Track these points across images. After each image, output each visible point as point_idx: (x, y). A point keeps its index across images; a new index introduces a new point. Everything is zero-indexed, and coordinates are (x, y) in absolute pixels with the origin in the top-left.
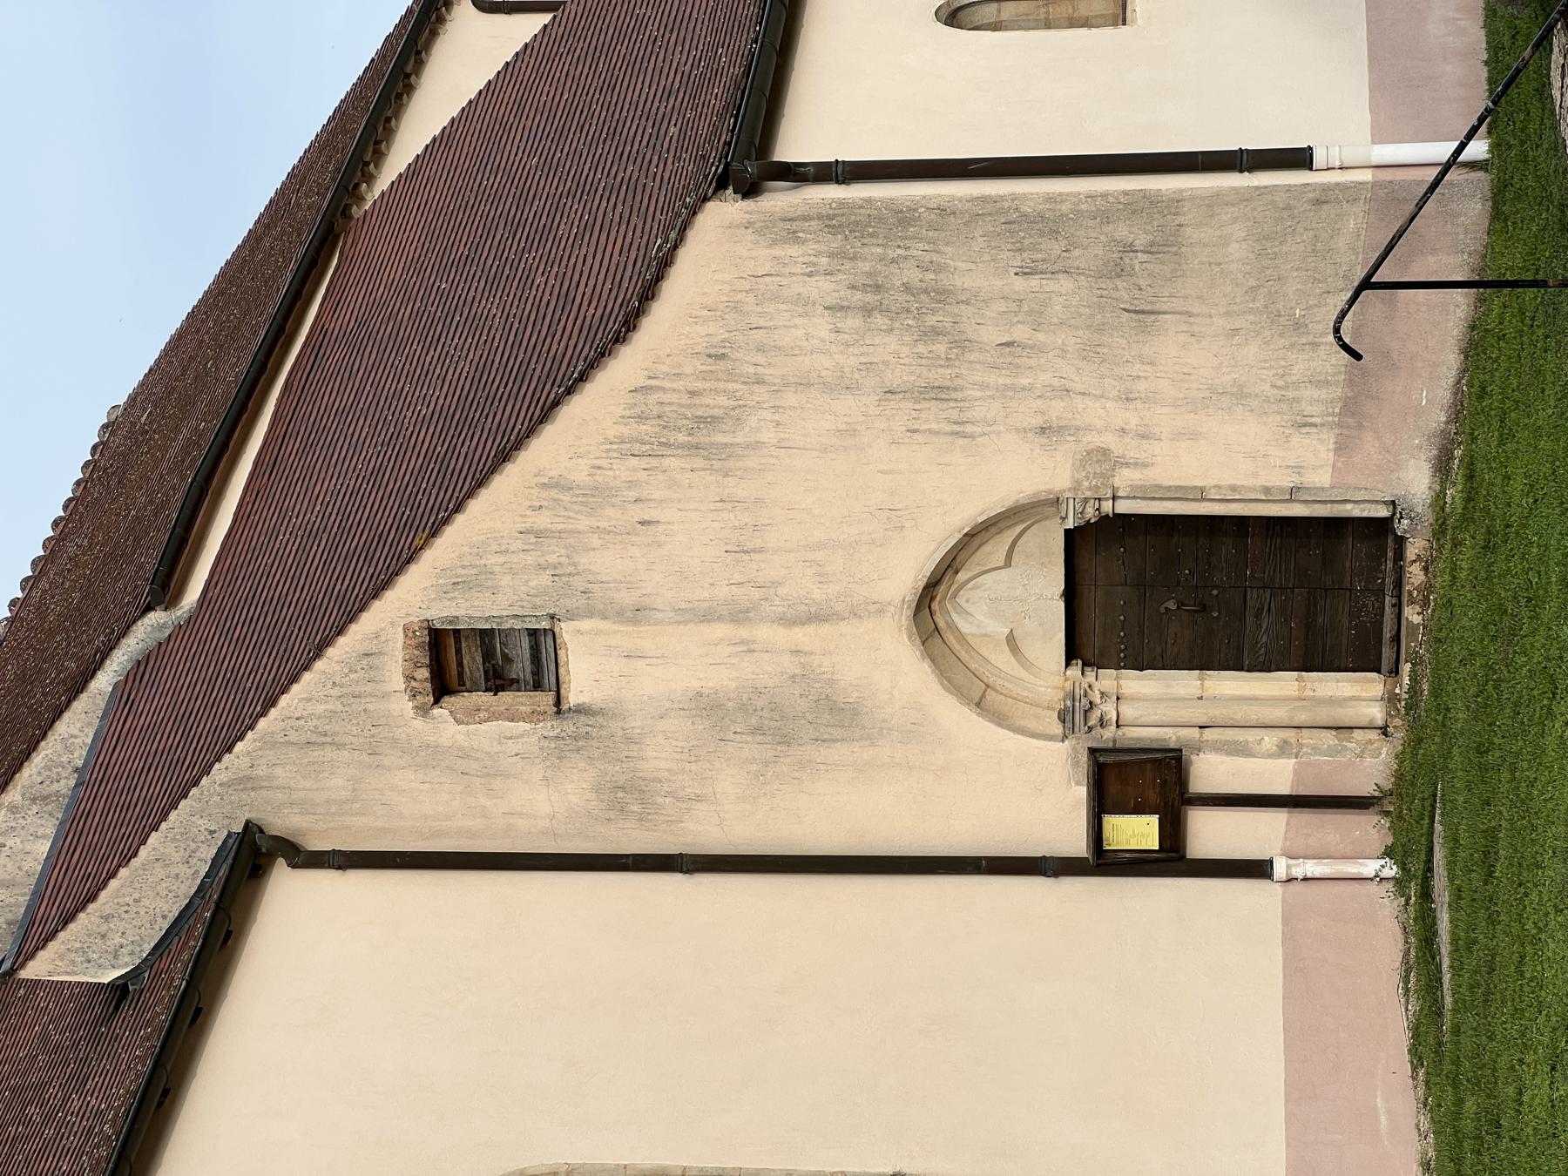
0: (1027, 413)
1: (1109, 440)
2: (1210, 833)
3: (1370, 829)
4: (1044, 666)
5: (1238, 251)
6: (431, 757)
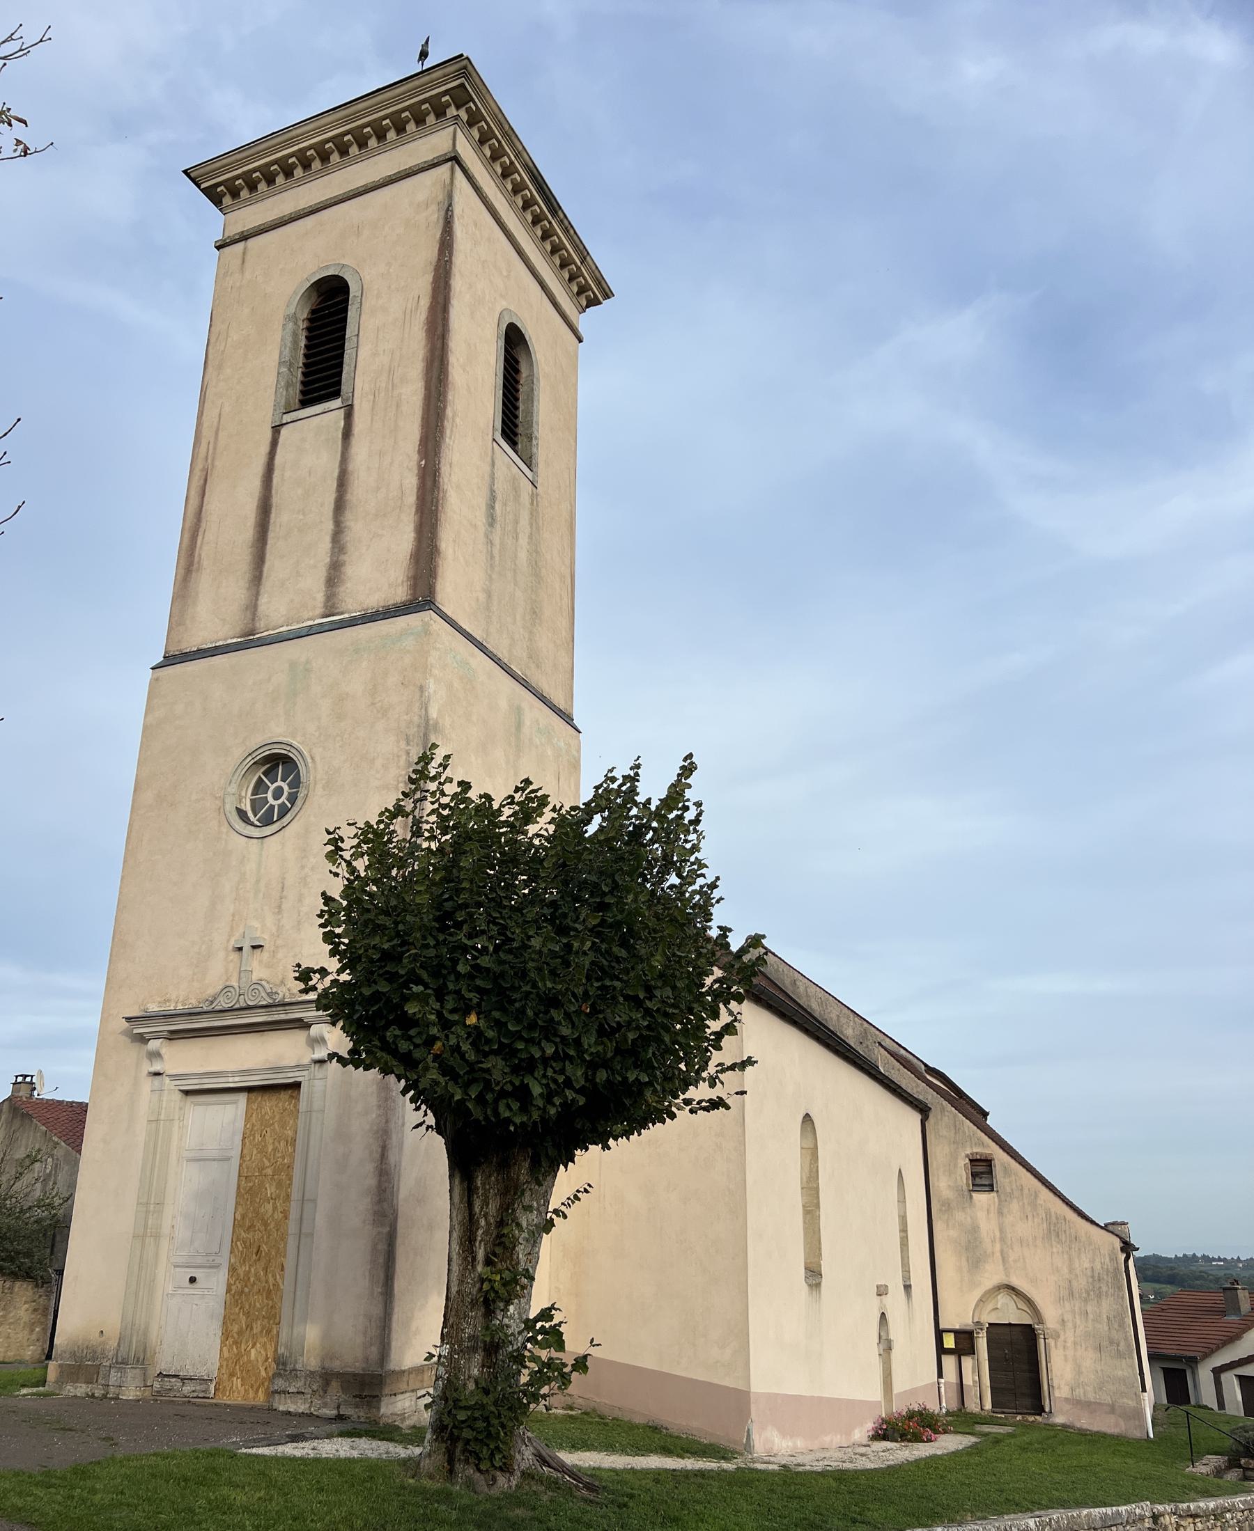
0: (1068, 1317)
1: (1062, 1338)
2: (949, 1362)
4: (988, 1318)
5: (1120, 1373)
6: (954, 1156)
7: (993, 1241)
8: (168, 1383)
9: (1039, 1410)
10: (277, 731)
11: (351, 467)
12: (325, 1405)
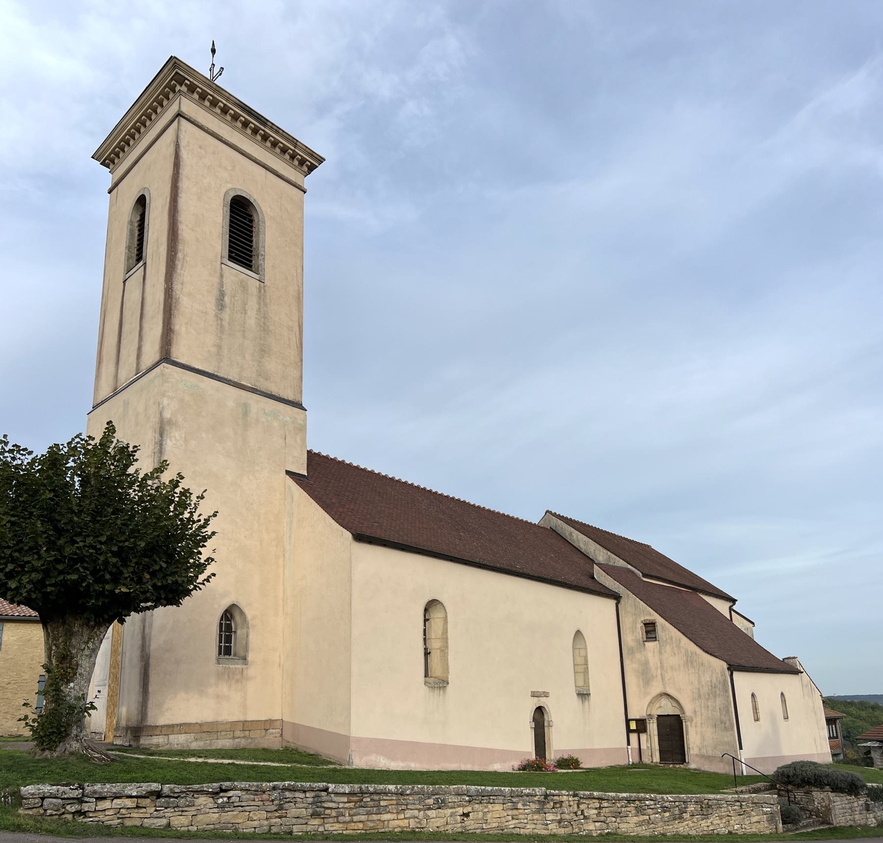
2: (634, 737)
3: (637, 760)
5: (726, 739)
6: (635, 622)
7: (657, 669)
9: (683, 761)
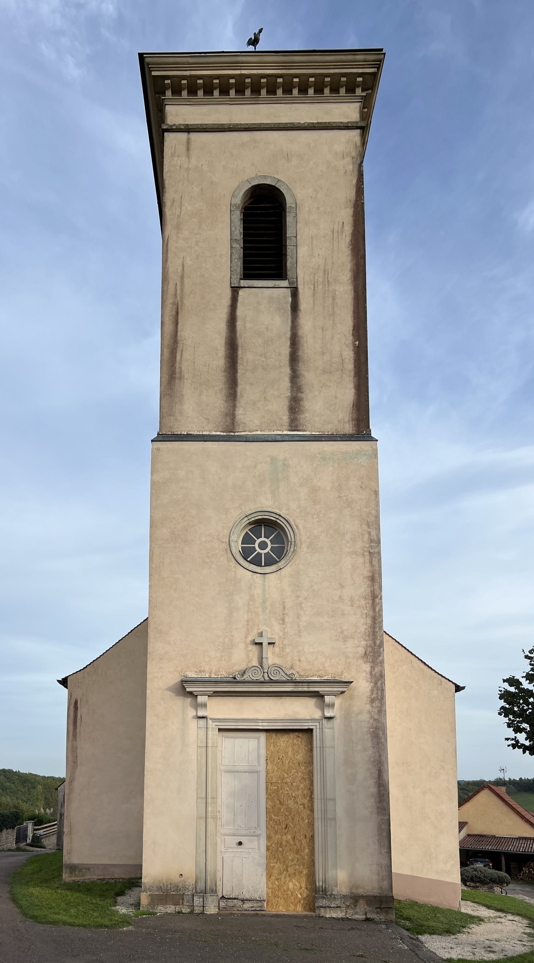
8: (231, 903)
10: (266, 504)
11: (300, 333)
12: (356, 913)
